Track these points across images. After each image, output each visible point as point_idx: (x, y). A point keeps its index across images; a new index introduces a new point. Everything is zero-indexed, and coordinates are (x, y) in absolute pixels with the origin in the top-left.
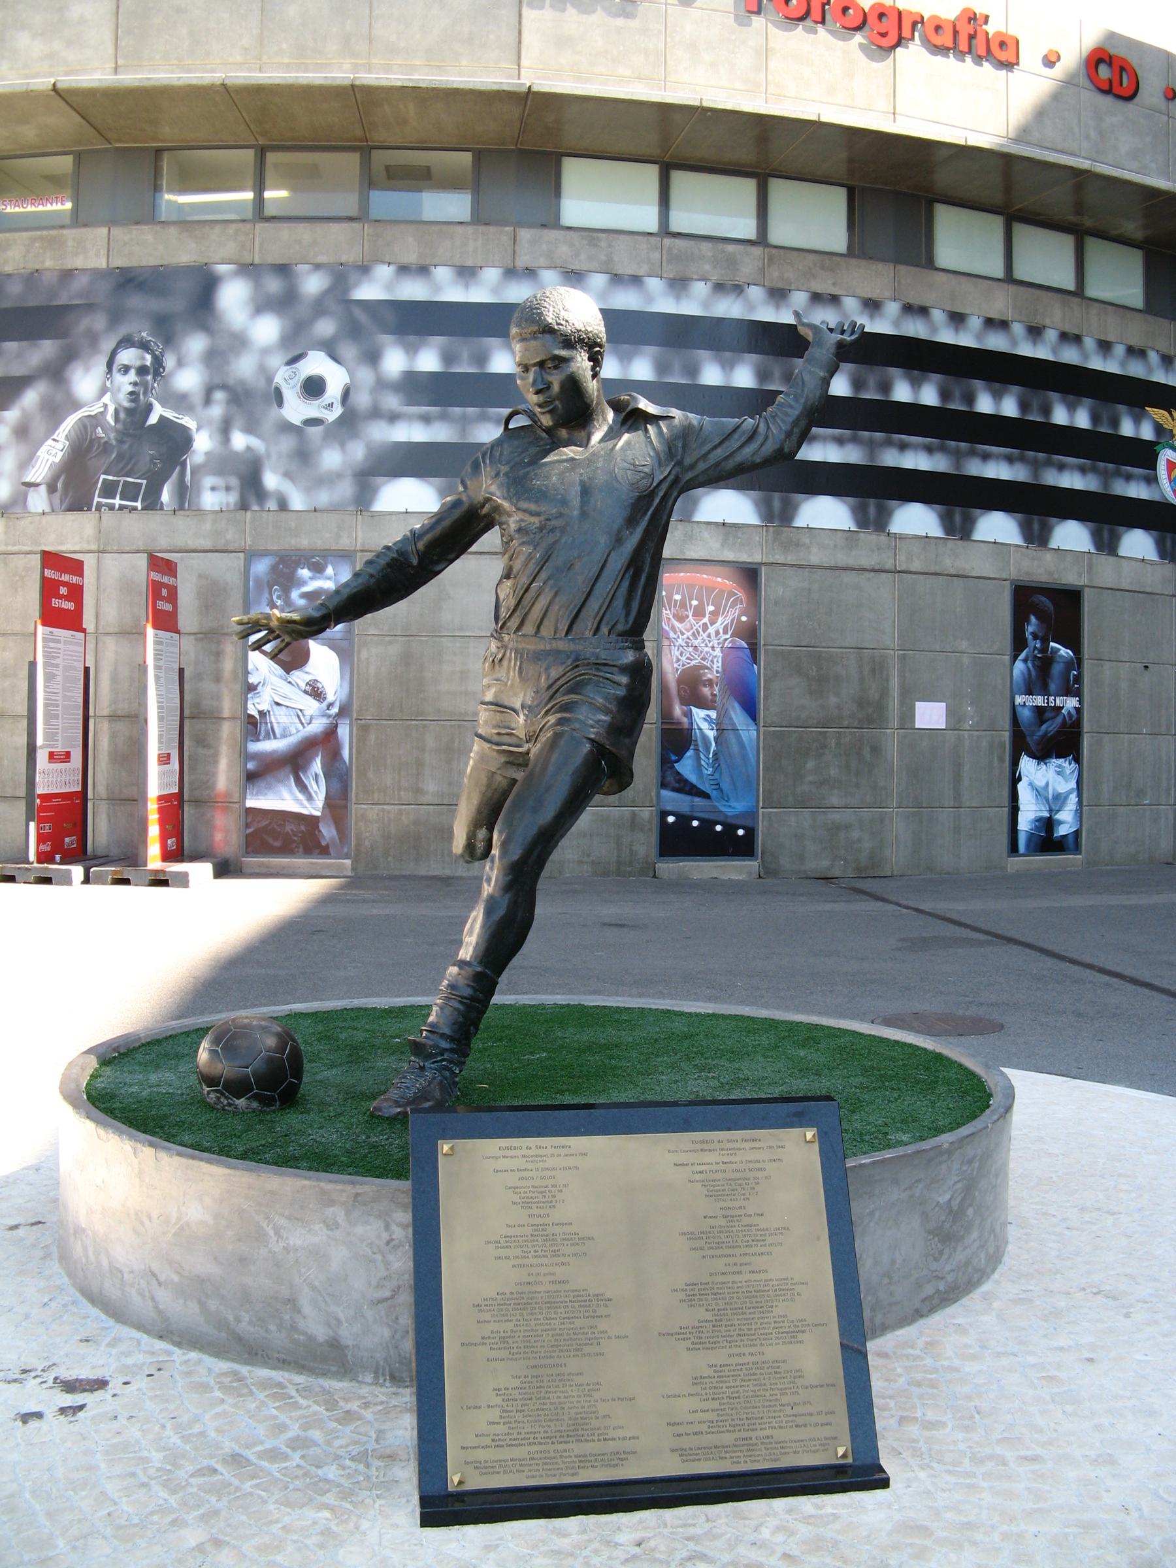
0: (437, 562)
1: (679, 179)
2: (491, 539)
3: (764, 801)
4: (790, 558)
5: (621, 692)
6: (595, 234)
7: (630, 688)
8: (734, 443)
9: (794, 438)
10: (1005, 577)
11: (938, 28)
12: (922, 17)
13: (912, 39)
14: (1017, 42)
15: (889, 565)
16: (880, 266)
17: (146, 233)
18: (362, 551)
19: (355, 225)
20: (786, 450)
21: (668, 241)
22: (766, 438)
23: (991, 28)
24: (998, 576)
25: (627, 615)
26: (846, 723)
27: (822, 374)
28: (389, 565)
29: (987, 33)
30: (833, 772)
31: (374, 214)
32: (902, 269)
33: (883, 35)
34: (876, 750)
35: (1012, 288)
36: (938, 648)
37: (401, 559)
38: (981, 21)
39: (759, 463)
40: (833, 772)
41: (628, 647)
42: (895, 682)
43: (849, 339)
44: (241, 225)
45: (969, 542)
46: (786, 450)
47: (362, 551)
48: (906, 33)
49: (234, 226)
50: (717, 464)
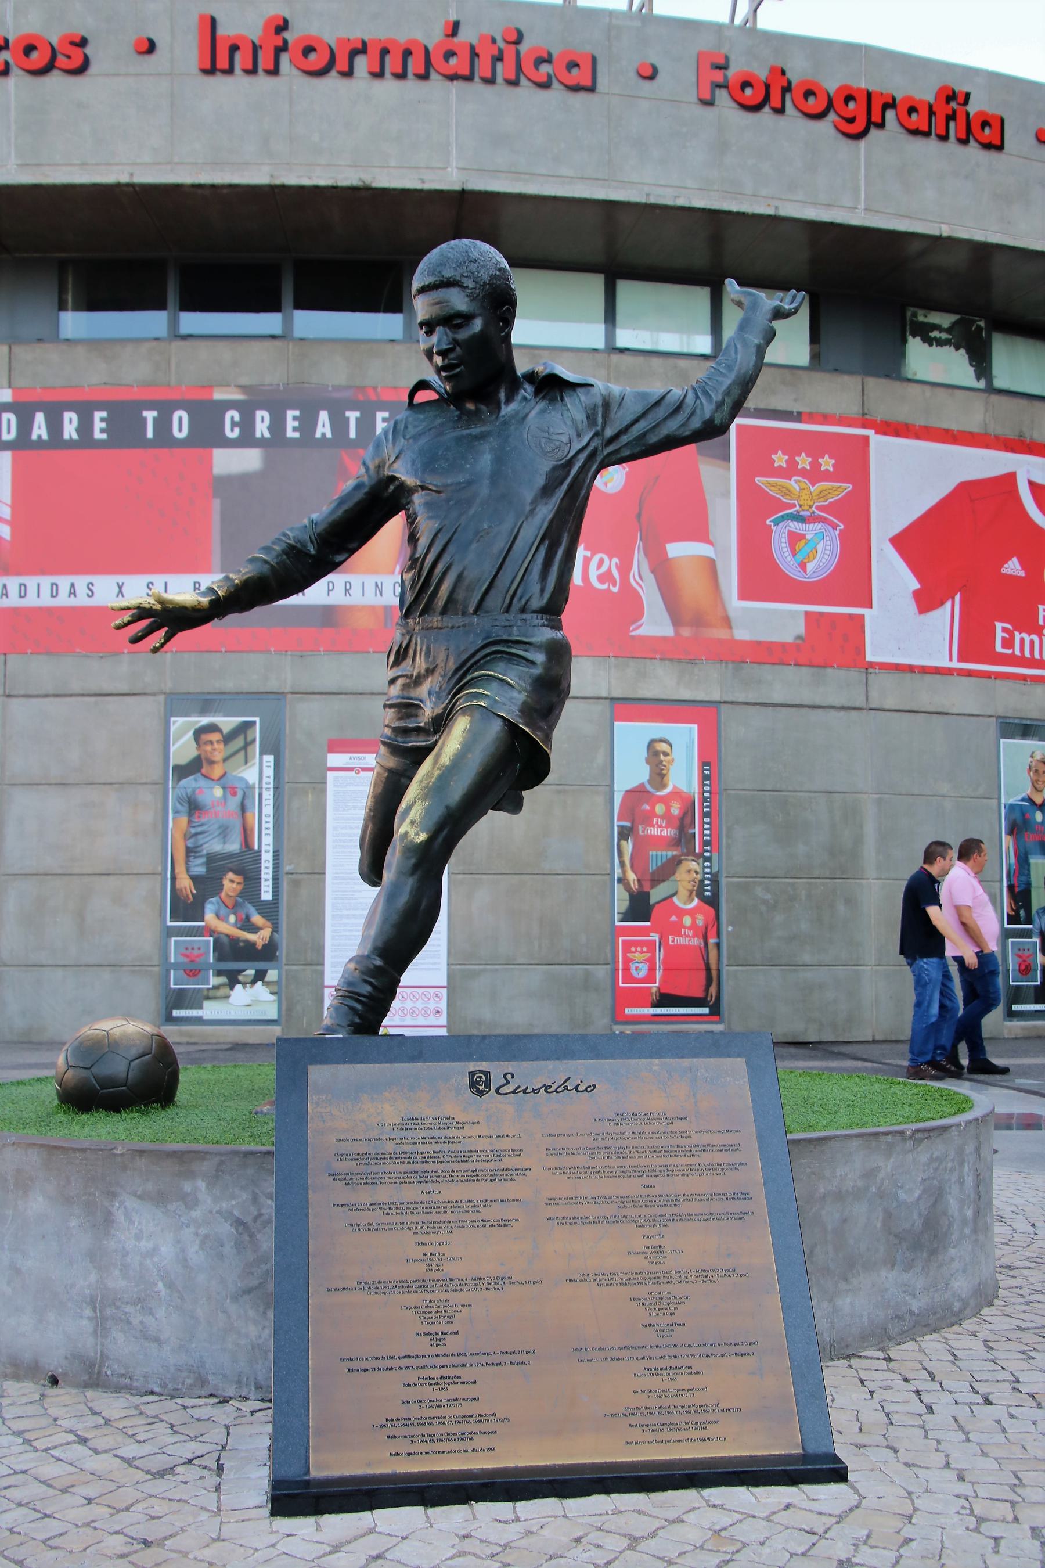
0: (339, 552)
1: (625, 289)
2: (394, 528)
3: (729, 958)
4: (752, 697)
5: (537, 671)
6: (537, 352)
7: (548, 666)
8: (661, 412)
9: (726, 409)
10: (989, 713)
11: (912, 110)
12: (894, 99)
13: (881, 125)
14: (1002, 121)
15: (860, 702)
16: (846, 379)
17: (51, 353)
18: (293, 693)
19: (277, 343)
20: (717, 422)
21: (615, 358)
22: (693, 414)
23: (973, 108)
24: (982, 713)
25: (542, 591)
26: (816, 873)
27: (756, 341)
28: (284, 552)
29: (968, 114)
30: (804, 926)
31: (298, 333)
32: (871, 382)
33: (851, 121)
34: (850, 902)
35: (995, 398)
36: (916, 792)
37: (299, 545)
38: (961, 100)
39: (688, 437)
40: (804, 926)
41: (543, 625)
42: (870, 830)
43: (787, 307)
44: (154, 343)
45: (897, 385)
46: (717, 422)
47: (293, 693)
48: (876, 118)
49: (147, 345)
50: (644, 435)
